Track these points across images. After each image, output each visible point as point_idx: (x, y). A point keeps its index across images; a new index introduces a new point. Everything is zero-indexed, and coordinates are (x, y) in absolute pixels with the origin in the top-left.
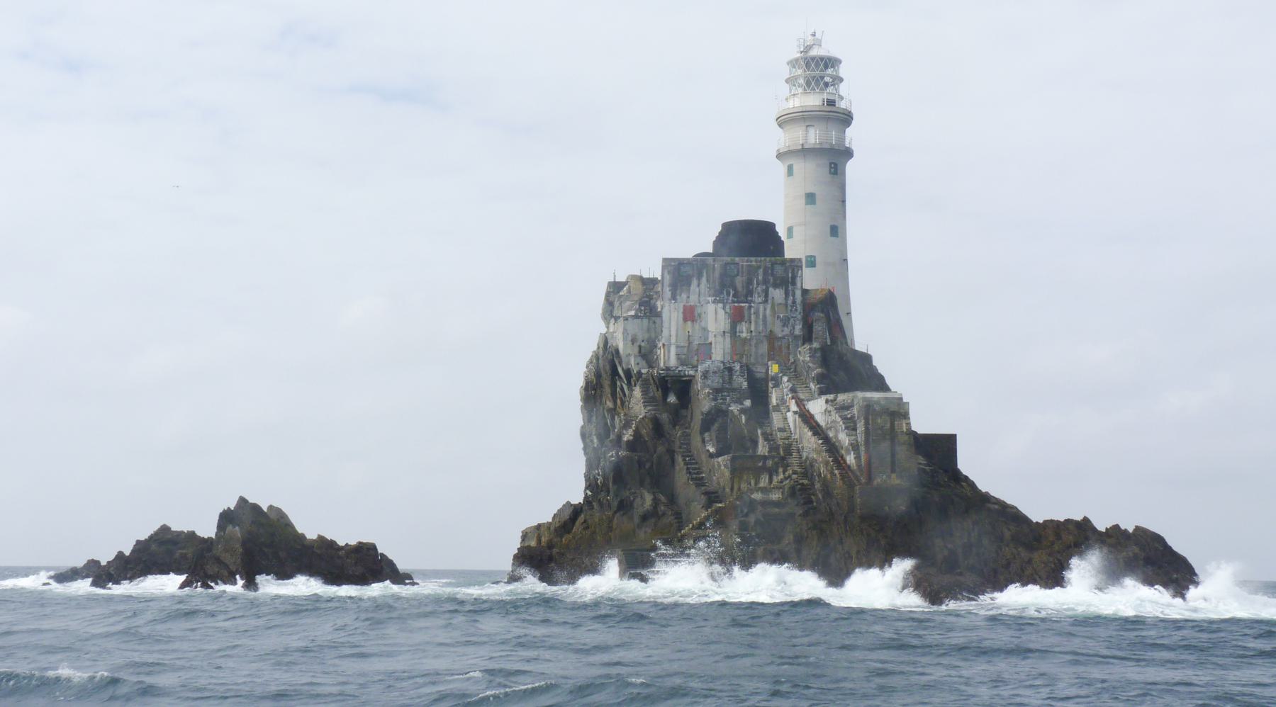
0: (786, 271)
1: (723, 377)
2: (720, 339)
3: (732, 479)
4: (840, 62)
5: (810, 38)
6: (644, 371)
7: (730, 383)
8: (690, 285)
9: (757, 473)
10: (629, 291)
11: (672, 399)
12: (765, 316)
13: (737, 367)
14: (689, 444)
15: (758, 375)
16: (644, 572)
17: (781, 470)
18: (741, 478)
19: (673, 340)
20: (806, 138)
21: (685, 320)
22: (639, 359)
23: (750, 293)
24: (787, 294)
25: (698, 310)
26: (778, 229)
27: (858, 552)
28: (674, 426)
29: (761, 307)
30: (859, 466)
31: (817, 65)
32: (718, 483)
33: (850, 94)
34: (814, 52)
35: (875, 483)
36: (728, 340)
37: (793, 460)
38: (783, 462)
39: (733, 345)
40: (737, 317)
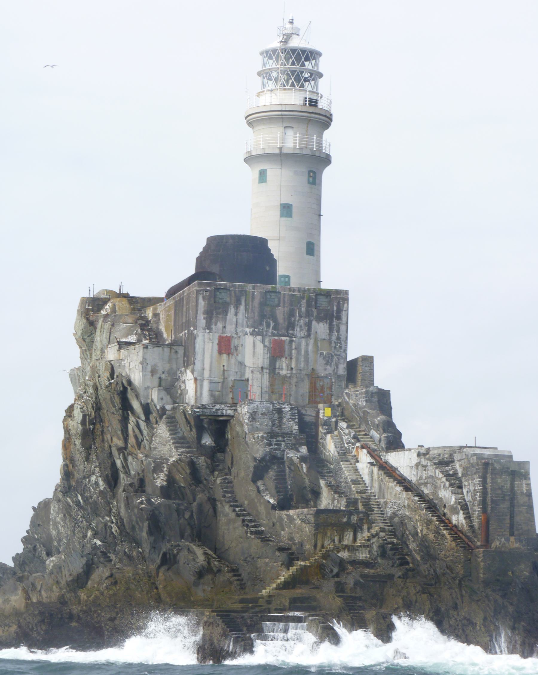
0: (330, 303)
1: (272, 419)
2: (258, 375)
3: (316, 535)
4: (320, 54)
5: (288, 26)
6: (168, 407)
8: (226, 313)
9: (341, 529)
10: (114, 310)
11: (207, 441)
12: (307, 352)
13: (287, 409)
14: (232, 492)
15: (308, 419)
17: (365, 527)
18: (325, 534)
19: (206, 374)
20: (283, 141)
21: (220, 352)
22: (163, 394)
23: (291, 326)
24: (331, 329)
25: (235, 342)
26: (270, 245)
27: (485, 619)
28: (212, 472)
29: (303, 342)
30: (472, 527)
31: (298, 58)
32: (291, 539)
33: (330, 92)
34: (295, 43)
35: (493, 545)
36: (266, 376)
37: (375, 516)
38: (366, 518)
39: (272, 385)
40: (276, 352)
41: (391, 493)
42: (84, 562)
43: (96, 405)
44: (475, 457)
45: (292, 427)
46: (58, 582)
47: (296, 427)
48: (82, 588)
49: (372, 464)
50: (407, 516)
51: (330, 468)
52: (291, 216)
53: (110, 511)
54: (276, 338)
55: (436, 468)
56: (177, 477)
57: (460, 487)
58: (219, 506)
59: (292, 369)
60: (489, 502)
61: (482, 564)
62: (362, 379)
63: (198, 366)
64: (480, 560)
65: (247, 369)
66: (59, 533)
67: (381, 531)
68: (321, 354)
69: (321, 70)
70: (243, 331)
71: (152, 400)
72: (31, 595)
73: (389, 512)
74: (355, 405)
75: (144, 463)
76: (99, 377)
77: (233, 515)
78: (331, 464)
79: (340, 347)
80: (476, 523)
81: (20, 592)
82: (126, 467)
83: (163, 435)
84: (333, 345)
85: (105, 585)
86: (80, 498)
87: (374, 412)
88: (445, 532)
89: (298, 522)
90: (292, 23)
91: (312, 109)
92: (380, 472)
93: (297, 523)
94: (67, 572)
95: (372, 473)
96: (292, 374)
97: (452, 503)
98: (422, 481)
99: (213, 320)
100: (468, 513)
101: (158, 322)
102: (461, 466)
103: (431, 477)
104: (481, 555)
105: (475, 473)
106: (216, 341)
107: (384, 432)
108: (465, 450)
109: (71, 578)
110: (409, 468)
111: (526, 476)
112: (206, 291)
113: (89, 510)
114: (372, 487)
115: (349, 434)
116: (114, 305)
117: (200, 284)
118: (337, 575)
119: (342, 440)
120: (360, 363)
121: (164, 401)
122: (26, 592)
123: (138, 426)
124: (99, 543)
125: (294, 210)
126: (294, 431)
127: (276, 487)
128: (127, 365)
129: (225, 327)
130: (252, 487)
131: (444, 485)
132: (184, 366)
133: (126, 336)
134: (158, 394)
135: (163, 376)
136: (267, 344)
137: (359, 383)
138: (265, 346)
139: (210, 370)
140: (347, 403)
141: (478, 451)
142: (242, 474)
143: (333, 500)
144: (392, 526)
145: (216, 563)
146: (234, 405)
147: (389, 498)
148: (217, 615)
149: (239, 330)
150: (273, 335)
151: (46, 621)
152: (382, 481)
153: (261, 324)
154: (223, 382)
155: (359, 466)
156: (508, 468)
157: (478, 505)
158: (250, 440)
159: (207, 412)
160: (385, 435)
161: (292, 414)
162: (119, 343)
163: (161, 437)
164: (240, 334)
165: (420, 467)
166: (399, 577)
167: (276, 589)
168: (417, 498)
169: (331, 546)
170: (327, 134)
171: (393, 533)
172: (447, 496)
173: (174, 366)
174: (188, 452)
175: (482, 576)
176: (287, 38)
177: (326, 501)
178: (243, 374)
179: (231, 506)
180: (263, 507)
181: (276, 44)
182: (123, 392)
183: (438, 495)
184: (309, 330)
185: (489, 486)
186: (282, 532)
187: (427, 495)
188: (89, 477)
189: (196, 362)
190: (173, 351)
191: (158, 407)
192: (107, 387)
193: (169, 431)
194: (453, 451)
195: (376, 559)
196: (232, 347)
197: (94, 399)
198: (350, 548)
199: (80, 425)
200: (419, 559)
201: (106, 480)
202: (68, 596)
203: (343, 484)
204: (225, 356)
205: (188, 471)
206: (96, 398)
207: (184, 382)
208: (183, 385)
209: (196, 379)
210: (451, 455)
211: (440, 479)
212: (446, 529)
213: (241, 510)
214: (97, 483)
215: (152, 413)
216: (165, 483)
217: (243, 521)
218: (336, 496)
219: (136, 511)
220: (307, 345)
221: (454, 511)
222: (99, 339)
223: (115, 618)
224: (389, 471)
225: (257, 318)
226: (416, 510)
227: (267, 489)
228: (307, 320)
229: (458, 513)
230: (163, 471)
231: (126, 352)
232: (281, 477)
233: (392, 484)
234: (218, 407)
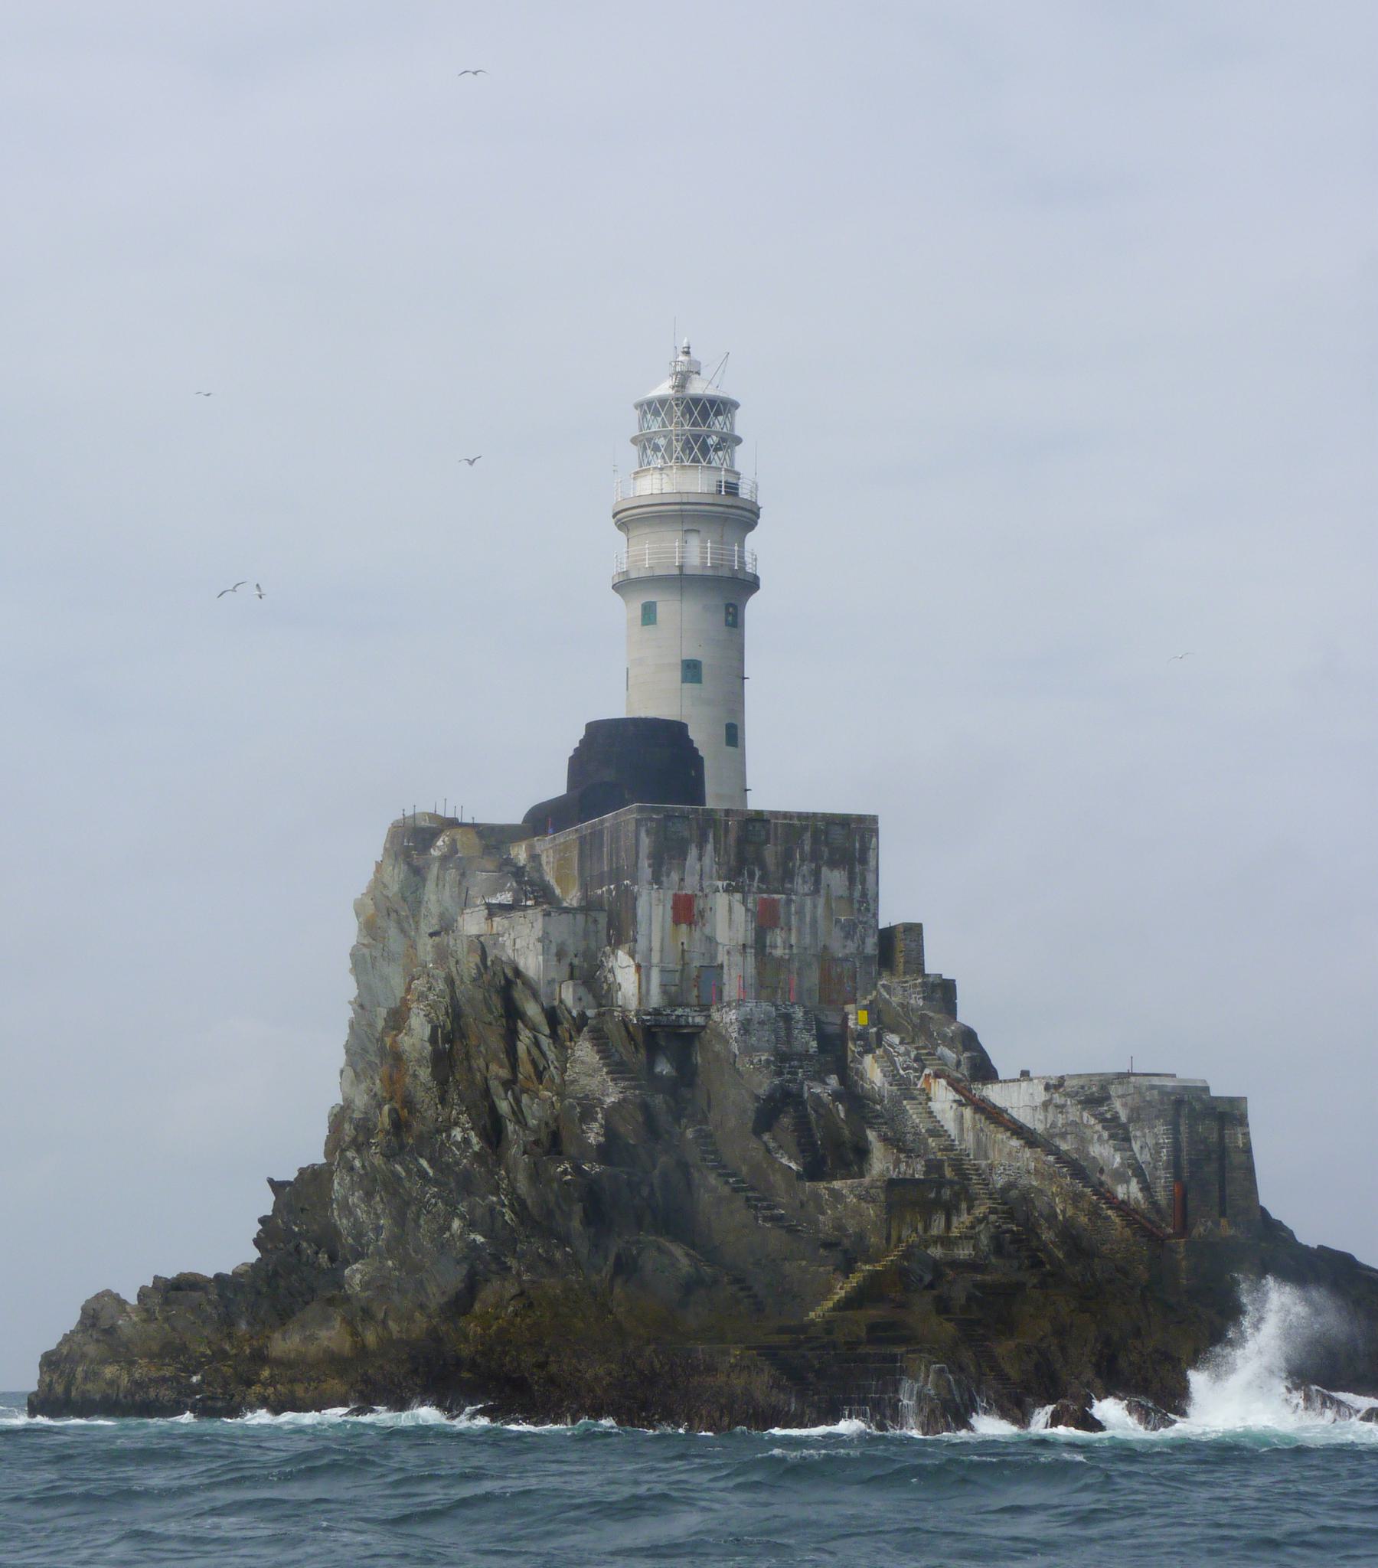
1: (775, 1031)
2: (737, 958)
4: (735, 405)
5: (682, 358)
6: (590, 1013)
7: (789, 1042)
8: (683, 855)
9: (927, 1209)
10: (453, 848)
11: (664, 1068)
12: (814, 921)
13: (799, 1014)
14: (715, 1152)
15: (831, 1029)
17: (964, 1206)
19: (655, 958)
21: (677, 921)
22: (582, 991)
23: (788, 875)
24: (851, 880)
25: (699, 904)
26: (693, 734)
28: (677, 1120)
29: (808, 901)
32: (840, 1228)
33: (755, 465)
34: (698, 388)
35: (1195, 1233)
36: (751, 960)
40: (765, 920)
41: (1000, 1151)
42: (464, 1272)
43: (454, 1010)
44: (1156, 1092)
45: (807, 1043)
46: (422, 1307)
47: (814, 1044)
48: (464, 1314)
49: (959, 1103)
50: (1033, 1186)
51: (874, 1111)
52: (699, 681)
53: (498, 1187)
54: (765, 896)
55: (1084, 1109)
56: (622, 1129)
57: (1127, 1139)
58: (696, 1175)
59: (791, 946)
60: (1184, 1163)
61: (1184, 1263)
62: (906, 962)
63: (642, 944)
64: (1179, 1257)
65: (720, 948)
66: (357, 1223)
67: (991, 1213)
68: (838, 921)
69: (738, 432)
70: (711, 886)
71: (561, 1001)
72: (360, 1329)
73: (999, 1182)
74: (902, 1005)
75: (558, 1106)
76: (457, 962)
77: (725, 1191)
78: (875, 1102)
79: (867, 910)
80: (1162, 1197)
81: (337, 1323)
83: (587, 1059)
84: (856, 906)
85: (511, 1309)
86: (424, 1163)
87: (940, 1016)
88: (1110, 1212)
89: (852, 1199)
90: (688, 353)
91: (730, 501)
92: (977, 1116)
93: (848, 1201)
94: (435, 1290)
95: (960, 1119)
96: (791, 955)
97: (1116, 1165)
98: (1057, 1131)
99: (664, 869)
100: (1145, 1180)
101: (539, 868)
102: (1124, 1105)
103: (1074, 1123)
104: (1182, 1249)
105: (1157, 1117)
106: (669, 904)
107: (965, 1049)
108: (1133, 1079)
109: (445, 1299)
110: (1028, 1110)
111: (1242, 1120)
112: (652, 820)
113: (453, 1185)
114: (961, 1140)
115: (907, 1053)
116: (453, 841)
117: (641, 810)
118: (931, 1286)
119: (893, 1063)
120: (900, 936)
121: (584, 1003)
122: (349, 1322)
123: (537, 1043)
124: (480, 1239)
125: (705, 671)
126: (811, 1051)
127: (799, 1144)
128: (509, 943)
129: (682, 880)
130: (754, 1144)
131: (1100, 1137)
132: (610, 944)
133: (494, 894)
134: (574, 992)
135: (576, 962)
136: (750, 906)
137: (901, 967)
138: (747, 910)
139: (662, 951)
140: (887, 1002)
141: (1156, 1081)
142: (732, 1122)
143: (897, 1164)
144: (1005, 1204)
145: (708, 1270)
146: (704, 1008)
147: (995, 1156)
148: (759, 1355)
149: (706, 883)
150: (760, 891)
151: (421, 1369)
152: (982, 1130)
153: (740, 874)
154: (683, 970)
155: (935, 1106)
156: (1214, 1108)
157: (1165, 1169)
158: (744, 1065)
159: (663, 1020)
160: (967, 1054)
161: (806, 1022)
162: (489, 906)
163: (582, 1062)
164: (707, 891)
165: (1051, 1109)
166: (1034, 1287)
167: (834, 1309)
168: (1051, 1158)
169: (914, 1238)
170: (751, 539)
171: (1010, 1215)
172: (1105, 1154)
173: (593, 945)
174: (635, 1088)
175: (1185, 1282)
176: (683, 379)
177: (881, 1162)
178: (713, 957)
179: (720, 1175)
180: (778, 1177)
181: (665, 388)
182: (506, 987)
183: (1088, 1153)
184: (817, 882)
185: (1184, 1138)
186: (821, 1217)
187: (1066, 1152)
188: (448, 1130)
189: (639, 937)
190: (590, 920)
191: (575, 1013)
192: (474, 980)
193: (598, 1052)
194: (1106, 1082)
195: (986, 1258)
196: (695, 911)
197: (448, 999)
198: (946, 1241)
199: (427, 1045)
200: (1061, 1256)
201: (483, 1135)
202: (443, 1328)
203: (909, 1137)
204: (684, 927)
205: (641, 1119)
206: (452, 998)
207: (612, 970)
208: (609, 975)
209: (638, 967)
210: (1104, 1088)
211: (1091, 1127)
212: (1110, 1208)
213: (737, 1182)
214: (466, 1141)
215: (561, 1023)
216: (601, 1139)
217: (748, 1199)
218: (902, 1156)
219: (555, 1186)
220: (815, 907)
221: (1120, 1177)
222: (433, 898)
223: (546, 1363)
224: (994, 1115)
225: (733, 862)
226: (1051, 1178)
227: (780, 1147)
228: (813, 866)
229: (1128, 1182)
230: (596, 1120)
231: (506, 922)
232: (803, 1126)
233: (1002, 1136)
234: (679, 1012)
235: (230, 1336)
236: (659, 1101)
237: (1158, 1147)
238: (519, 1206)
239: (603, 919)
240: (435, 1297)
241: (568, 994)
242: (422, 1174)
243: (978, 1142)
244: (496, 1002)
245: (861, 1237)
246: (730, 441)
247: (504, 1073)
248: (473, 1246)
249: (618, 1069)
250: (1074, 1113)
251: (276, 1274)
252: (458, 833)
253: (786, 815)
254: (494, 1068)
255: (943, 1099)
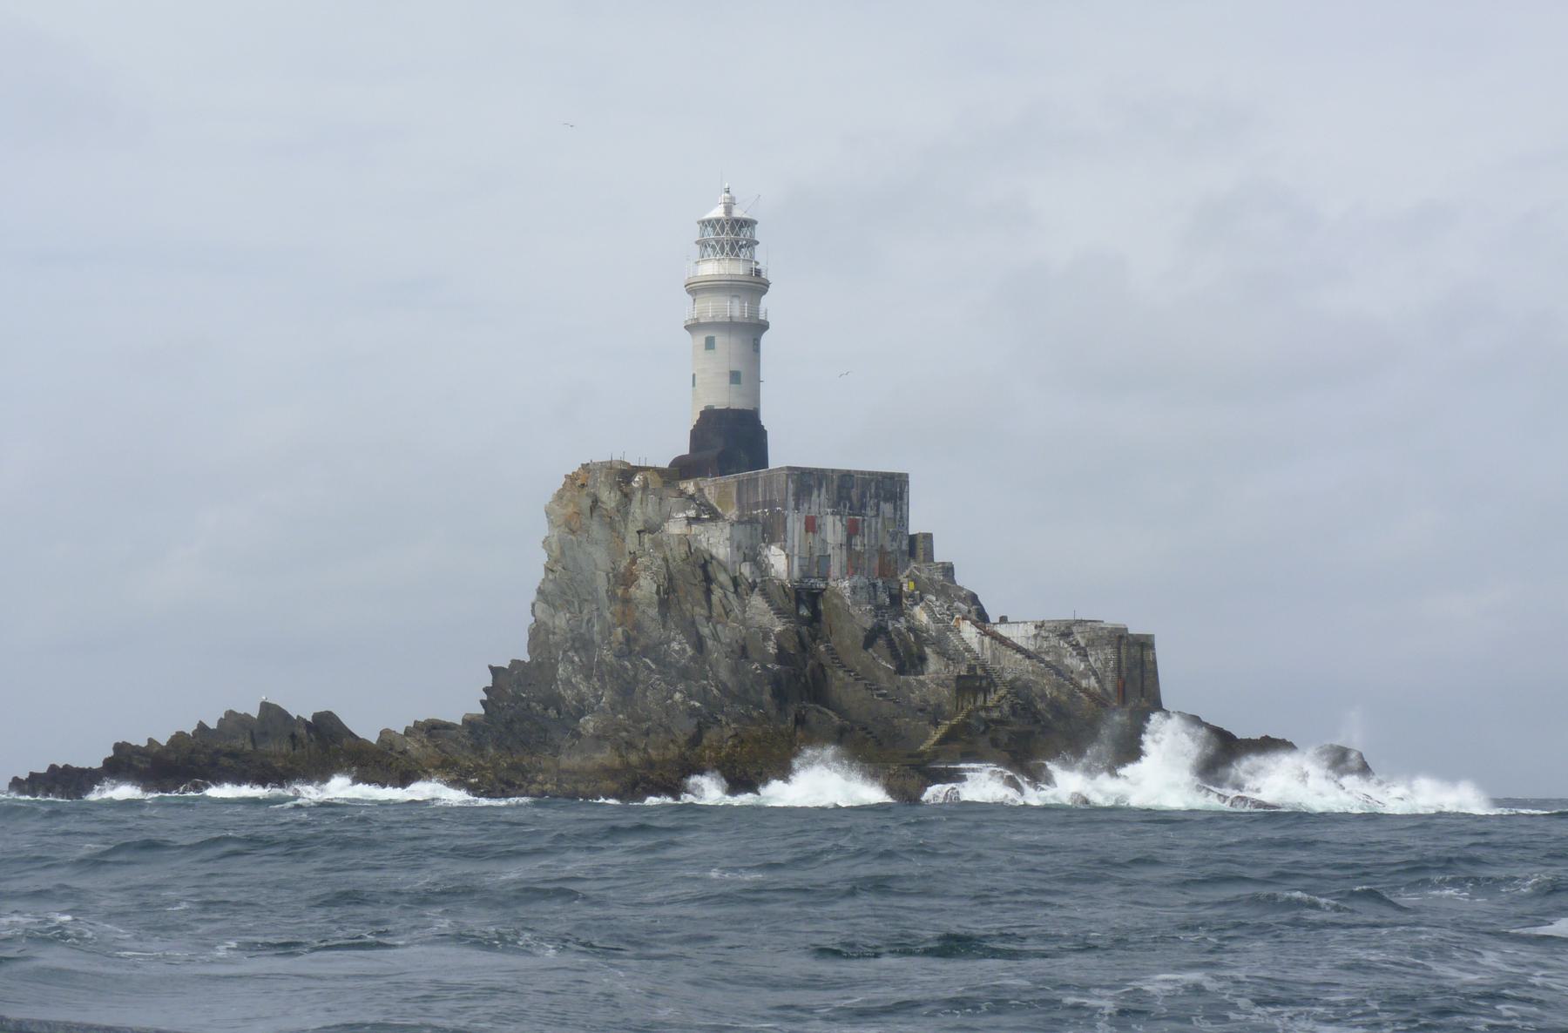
8: (810, 494)
9: (975, 691)
11: (804, 612)
16: (1026, 787)
23: (863, 506)
25: (818, 521)
28: (814, 640)
31: (732, 228)
32: (926, 701)
33: (767, 257)
34: (738, 213)
39: (849, 559)
40: (852, 530)
73: (1009, 677)
82: (715, 636)
95: (982, 643)
111: (1152, 647)
143: (947, 666)
147: (1005, 663)
158: (855, 611)
170: (765, 301)
171: (1017, 695)
176: (728, 209)
181: (718, 212)
182: (704, 566)
185: (1123, 655)
188: (668, 643)
214: (684, 650)
221: (1084, 675)
232: (891, 643)
233: (1010, 652)
235: (482, 756)
236: (804, 629)
237: (1107, 661)
238: (724, 689)
239: (760, 528)
240: (682, 739)
241: (746, 569)
242: (649, 668)
243: (994, 655)
244: (699, 572)
245: (939, 706)
246: (752, 243)
247: (704, 612)
248: (693, 708)
249: (780, 612)
250: (1054, 641)
251: (512, 721)
252: (648, 474)
253: (862, 473)
254: (697, 610)
255: (969, 632)
